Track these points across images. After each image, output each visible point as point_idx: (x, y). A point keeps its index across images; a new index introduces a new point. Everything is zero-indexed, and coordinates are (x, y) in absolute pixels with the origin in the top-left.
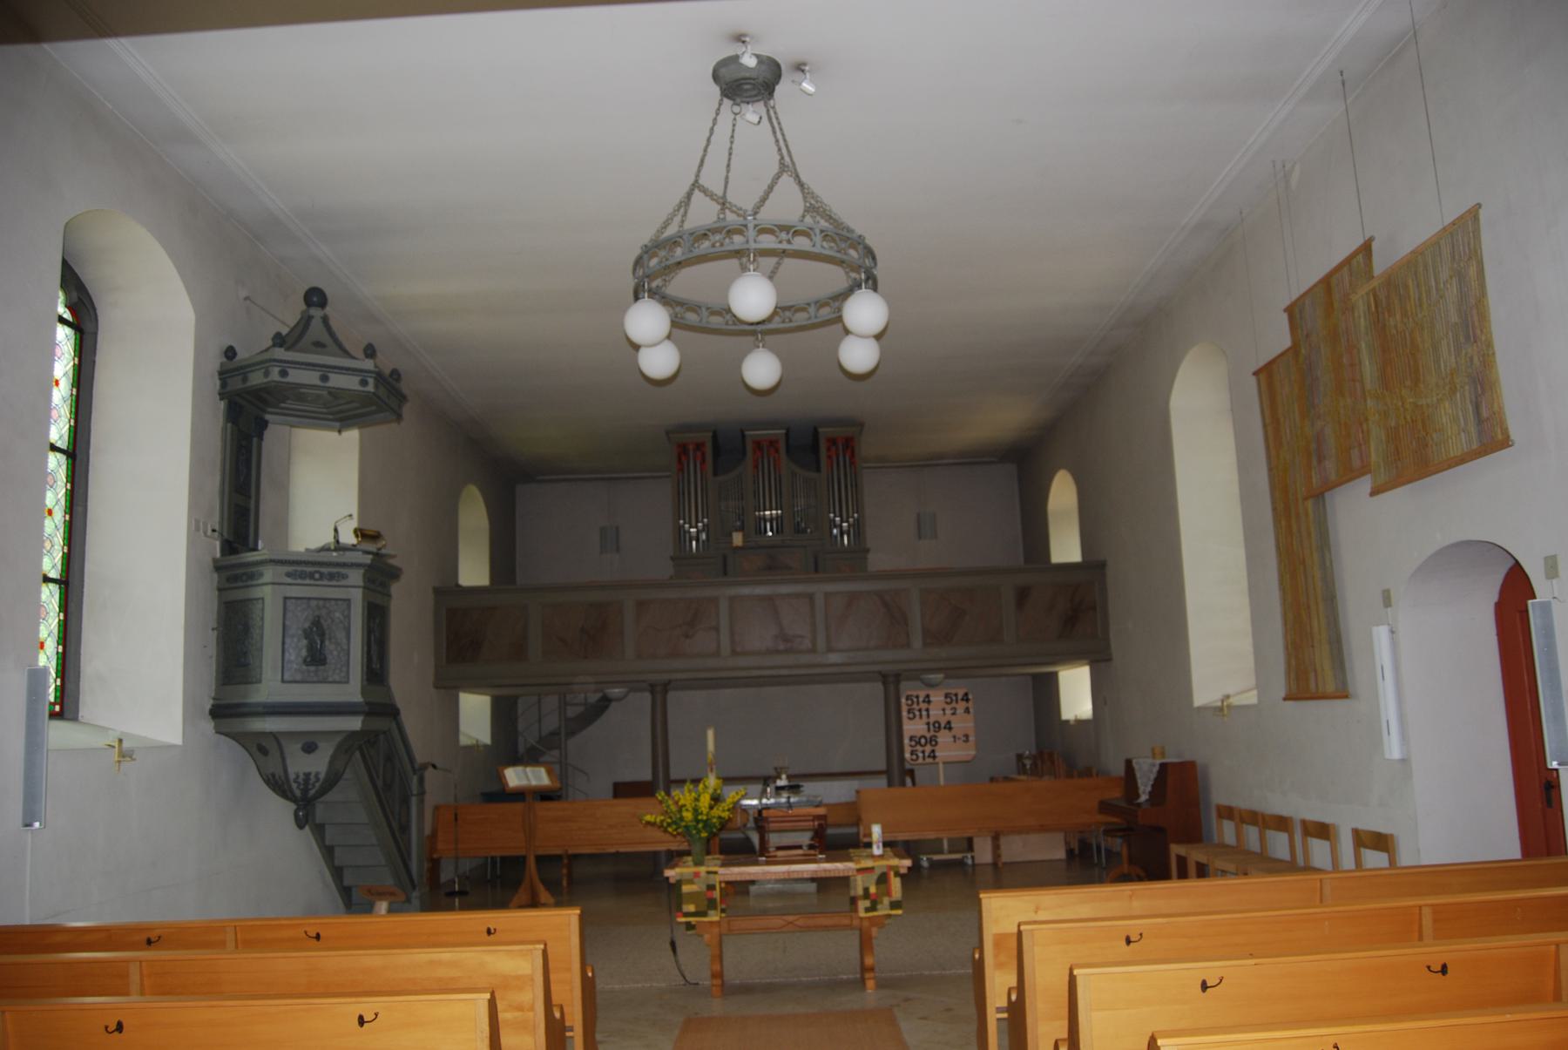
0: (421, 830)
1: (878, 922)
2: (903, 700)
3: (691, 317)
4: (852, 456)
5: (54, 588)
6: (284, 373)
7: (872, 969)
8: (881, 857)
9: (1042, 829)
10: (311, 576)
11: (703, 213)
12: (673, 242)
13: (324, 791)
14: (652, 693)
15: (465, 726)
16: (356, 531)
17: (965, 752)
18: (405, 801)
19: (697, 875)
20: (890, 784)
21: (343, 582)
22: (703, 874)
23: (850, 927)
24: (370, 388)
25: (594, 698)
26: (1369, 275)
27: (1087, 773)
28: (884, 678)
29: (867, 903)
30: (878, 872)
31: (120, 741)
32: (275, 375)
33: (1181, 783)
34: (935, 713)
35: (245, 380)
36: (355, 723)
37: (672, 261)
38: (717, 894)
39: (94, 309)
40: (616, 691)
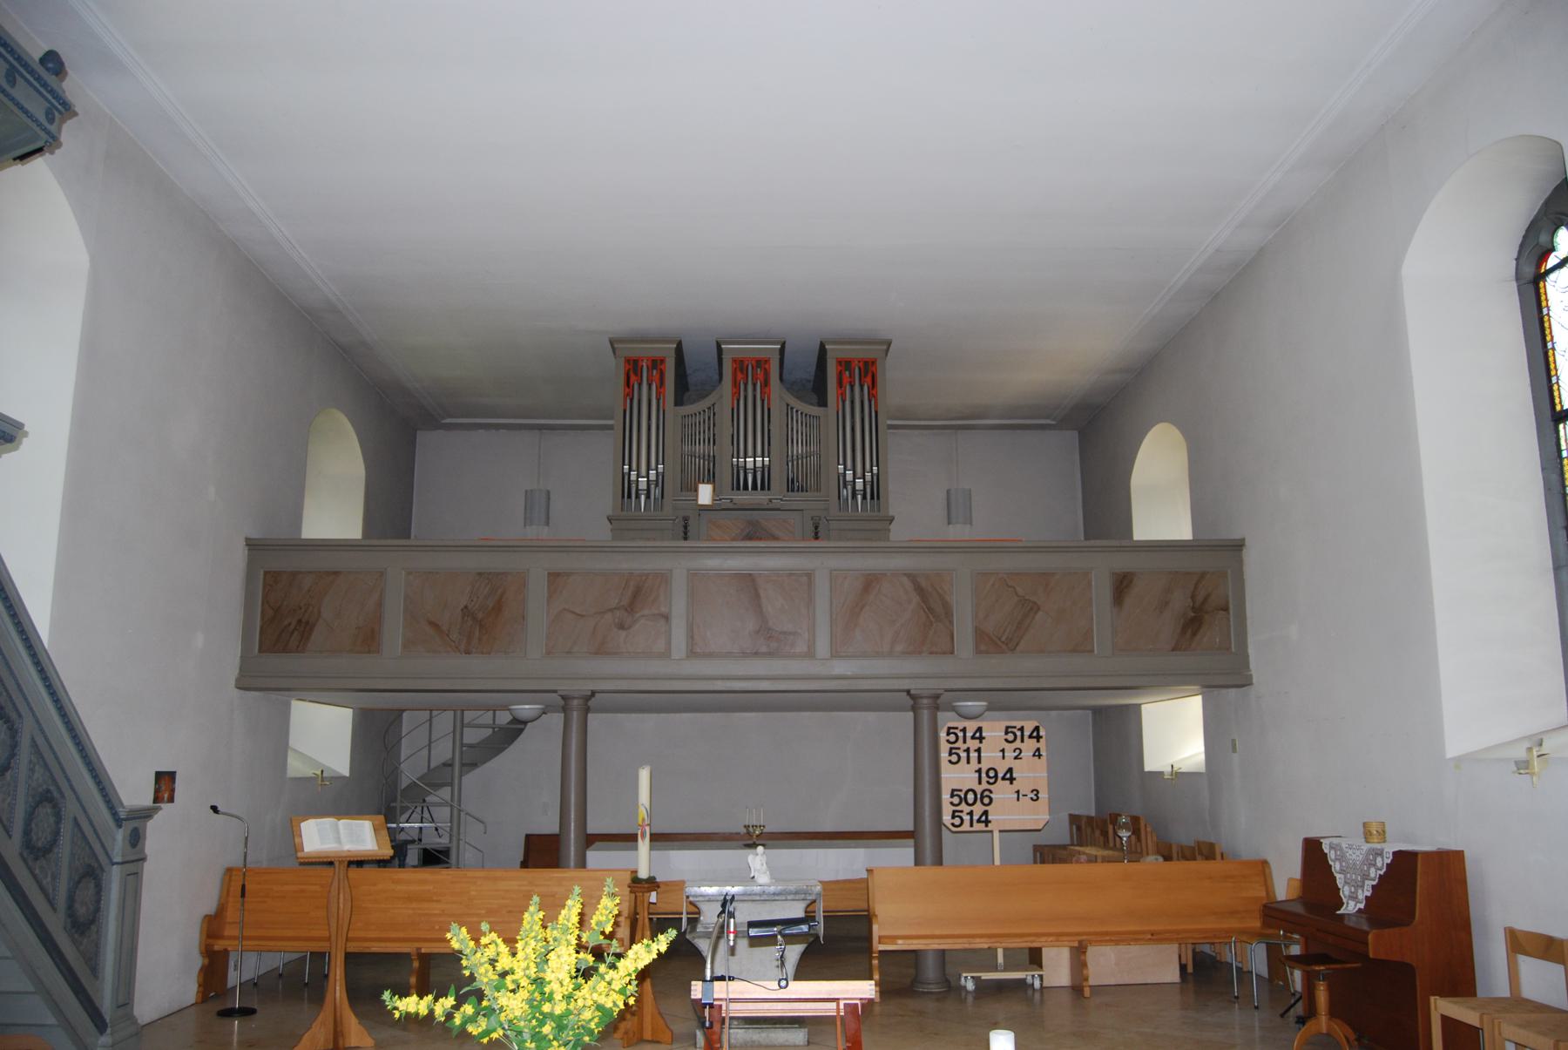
2: (943, 734)
9: (1156, 937)
17: (1035, 816)
18: (91, 874)
20: (918, 861)
25: (504, 718)
28: (914, 701)
34: (991, 757)
40: (525, 709)
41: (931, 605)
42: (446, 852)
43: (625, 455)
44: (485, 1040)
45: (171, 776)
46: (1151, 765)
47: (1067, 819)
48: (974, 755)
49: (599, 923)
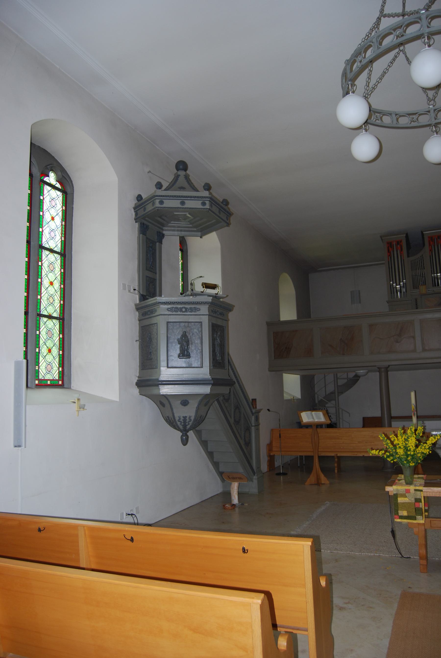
5: (56, 322)
6: (161, 202)
14: (379, 372)
18: (248, 429)
19: (408, 491)
21: (198, 313)
22: (412, 491)
24: (207, 206)
25: (351, 375)
31: (79, 399)
32: (157, 204)
35: (145, 210)
36: (206, 390)
38: (422, 505)
39: (72, 182)
40: (361, 372)
42: (336, 424)
44: (392, 462)
45: (255, 400)
49: (418, 433)
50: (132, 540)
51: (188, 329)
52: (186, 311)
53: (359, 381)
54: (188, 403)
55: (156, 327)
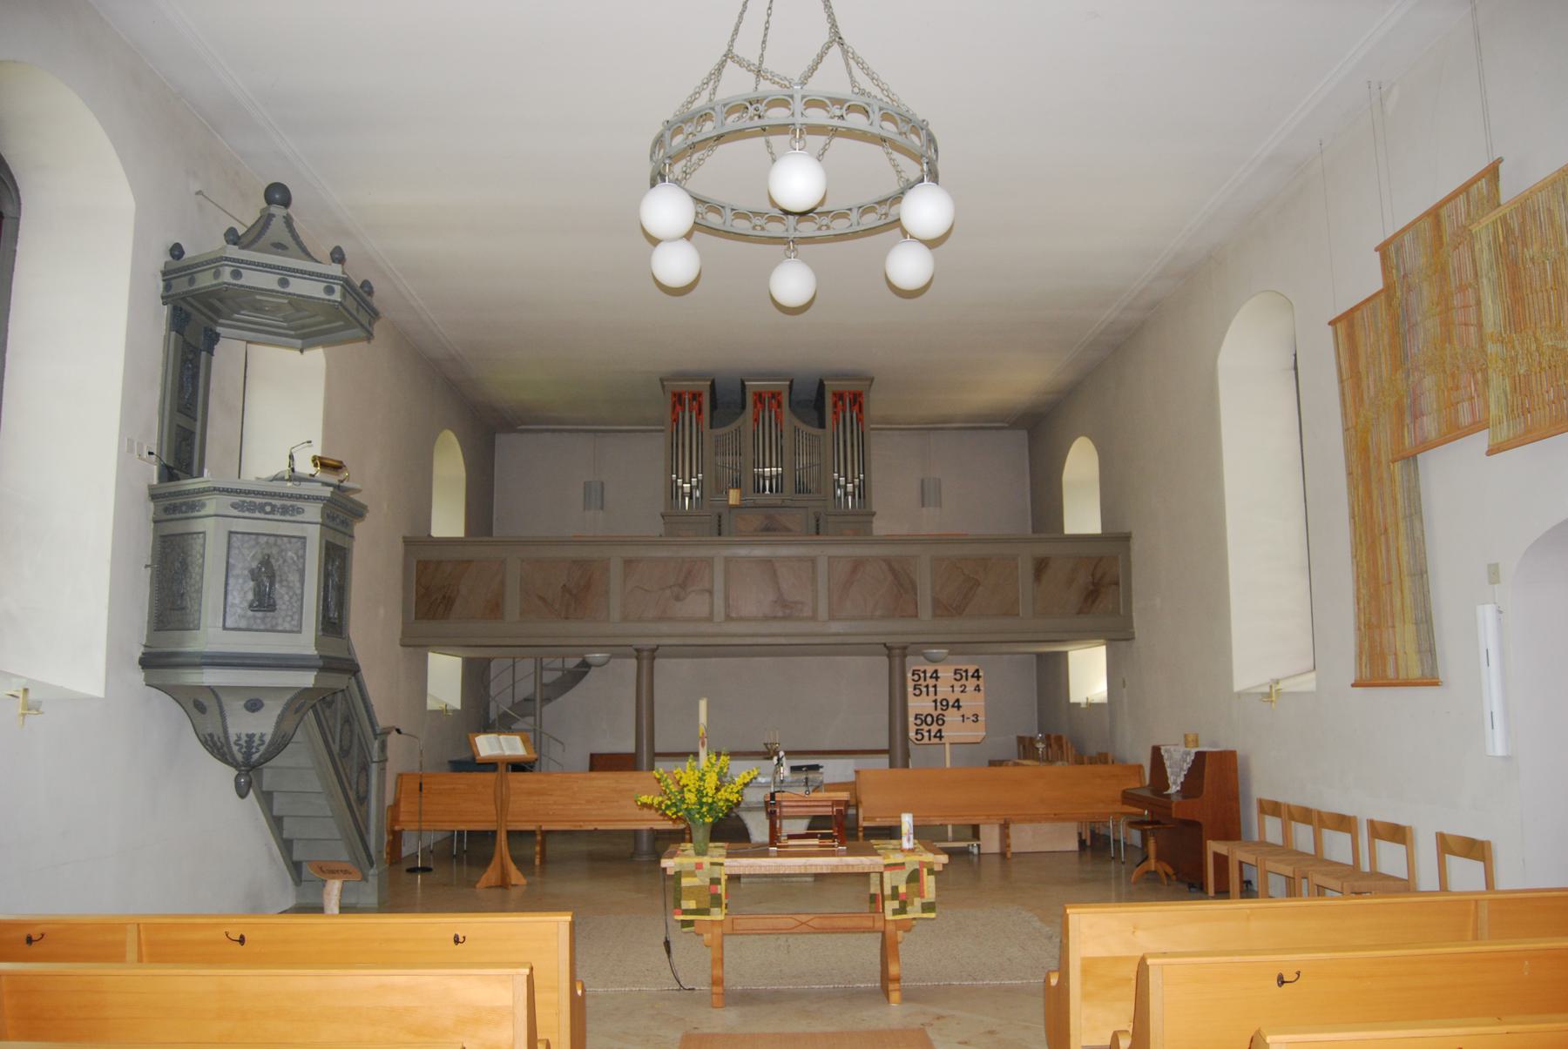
0: (381, 799)
1: (907, 927)
2: (909, 675)
3: (713, 219)
4: (861, 410)
6: (236, 274)
7: (897, 980)
8: (912, 851)
9: (1058, 818)
10: (261, 508)
11: (737, 84)
12: (705, 116)
13: (269, 756)
15: (433, 687)
16: (314, 459)
17: (976, 733)
18: (364, 768)
19: (699, 866)
20: (892, 765)
21: (299, 518)
22: (707, 866)
23: (871, 930)
24: (337, 297)
25: (572, 663)
26: (1493, 200)
27: (1102, 759)
28: (889, 650)
29: (896, 905)
30: (909, 869)
31: (26, 690)
32: (226, 276)
33: (1216, 775)
34: (944, 691)
35: (192, 281)
36: (307, 679)
37: (700, 137)
38: (721, 889)
39: (17, 190)
40: (596, 656)
41: (901, 585)
43: (673, 466)
46: (1073, 699)
47: (1014, 743)
48: (931, 690)
50: (242, 940)
51: (274, 551)
52: (272, 512)
53: (588, 677)
54: (262, 705)
55: (200, 541)
